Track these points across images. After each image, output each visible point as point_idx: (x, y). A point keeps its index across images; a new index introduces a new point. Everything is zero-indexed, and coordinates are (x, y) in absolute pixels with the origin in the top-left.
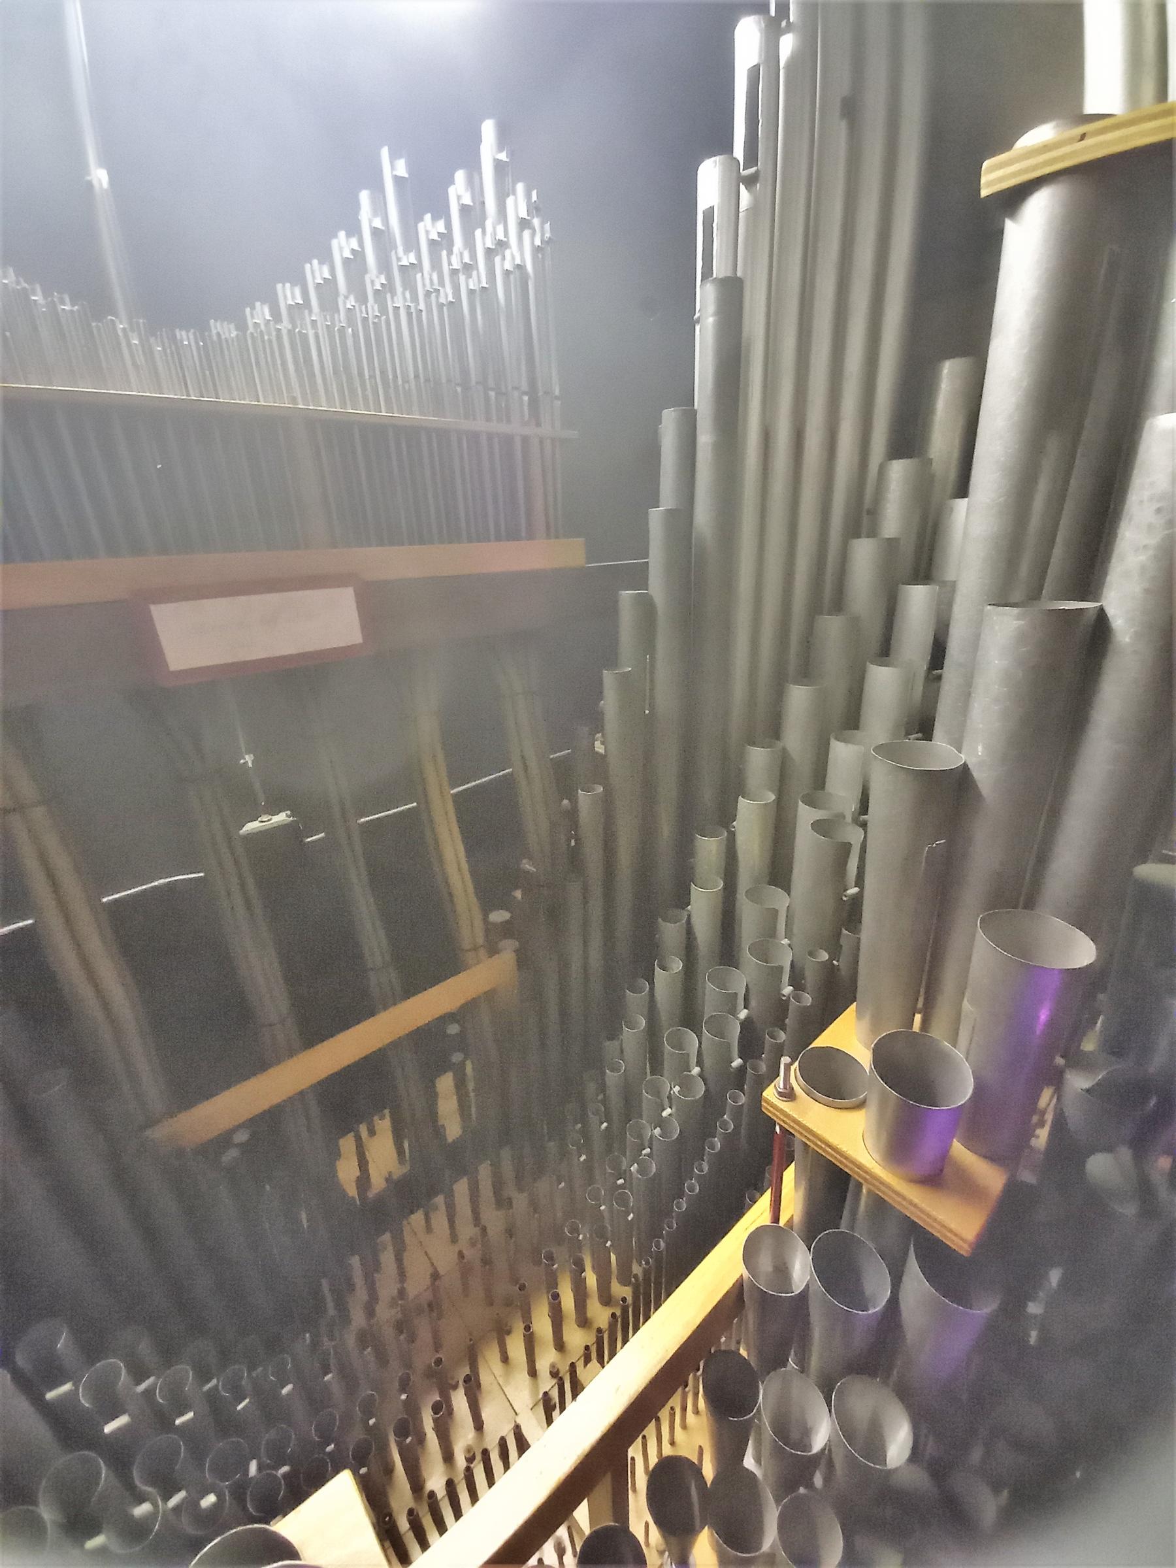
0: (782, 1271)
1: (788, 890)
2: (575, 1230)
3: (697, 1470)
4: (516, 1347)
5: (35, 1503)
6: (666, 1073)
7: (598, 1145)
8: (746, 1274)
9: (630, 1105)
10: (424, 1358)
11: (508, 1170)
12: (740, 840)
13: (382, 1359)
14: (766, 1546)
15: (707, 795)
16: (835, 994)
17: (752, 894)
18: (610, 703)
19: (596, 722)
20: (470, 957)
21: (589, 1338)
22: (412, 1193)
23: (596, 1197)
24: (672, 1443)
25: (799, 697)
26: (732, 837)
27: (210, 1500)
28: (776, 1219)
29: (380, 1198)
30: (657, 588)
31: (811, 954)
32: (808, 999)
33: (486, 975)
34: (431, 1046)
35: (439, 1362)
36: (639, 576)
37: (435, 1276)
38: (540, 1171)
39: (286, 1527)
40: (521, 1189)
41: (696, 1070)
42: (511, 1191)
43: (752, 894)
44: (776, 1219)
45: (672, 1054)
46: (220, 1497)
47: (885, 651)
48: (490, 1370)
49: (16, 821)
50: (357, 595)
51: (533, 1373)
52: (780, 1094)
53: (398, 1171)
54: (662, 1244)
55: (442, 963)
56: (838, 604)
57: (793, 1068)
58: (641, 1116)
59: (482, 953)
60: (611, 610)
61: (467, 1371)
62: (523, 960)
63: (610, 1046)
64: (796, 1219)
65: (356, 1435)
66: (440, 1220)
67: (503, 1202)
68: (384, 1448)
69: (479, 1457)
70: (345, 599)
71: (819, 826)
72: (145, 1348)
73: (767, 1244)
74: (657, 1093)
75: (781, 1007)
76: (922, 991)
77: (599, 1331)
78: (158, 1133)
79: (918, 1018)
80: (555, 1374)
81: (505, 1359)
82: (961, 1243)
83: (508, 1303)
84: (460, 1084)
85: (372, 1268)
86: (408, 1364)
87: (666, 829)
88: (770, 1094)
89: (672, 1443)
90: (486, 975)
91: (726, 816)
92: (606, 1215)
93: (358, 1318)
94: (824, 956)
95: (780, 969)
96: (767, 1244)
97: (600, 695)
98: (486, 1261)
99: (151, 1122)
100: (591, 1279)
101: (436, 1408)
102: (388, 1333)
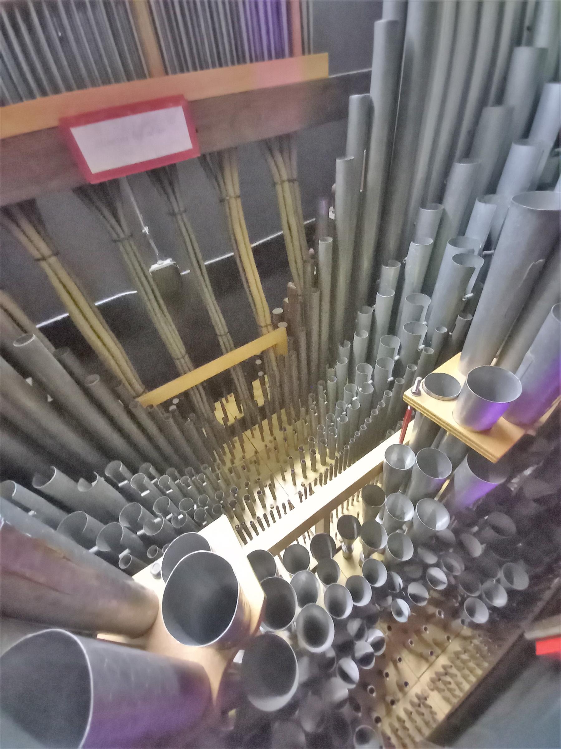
0: (401, 461)
1: (430, 295)
2: (312, 440)
3: (357, 520)
4: (288, 476)
5: (117, 520)
6: (356, 382)
7: (322, 410)
8: (385, 461)
9: (338, 397)
10: (254, 477)
11: (284, 417)
12: (408, 268)
13: (239, 477)
14: (382, 547)
15: (392, 243)
16: (448, 348)
17: (411, 298)
18: (339, 186)
19: (331, 198)
20: (264, 330)
21: (317, 475)
22: (245, 424)
23: (321, 428)
24: (348, 509)
25: (461, 171)
26: (403, 266)
27: (181, 516)
28: (402, 441)
29: (233, 425)
30: (377, 91)
31: (438, 329)
32: (432, 351)
33: (272, 339)
34: (251, 369)
35: (259, 479)
36: (362, 83)
37: (256, 452)
38: (298, 418)
39: (202, 533)
40: (290, 424)
41: (371, 382)
42: (285, 425)
43: (411, 298)
44: (402, 441)
45: (359, 374)
46: (185, 516)
47: (526, 134)
48: (278, 482)
49: (43, 264)
50: (183, 108)
51: (295, 484)
52: (413, 393)
53: (239, 416)
54: (349, 447)
55: (245, 331)
56: (500, 100)
57: (422, 381)
58: (343, 399)
59: (270, 328)
60: (342, 114)
61: (269, 482)
62: (290, 331)
63: (330, 371)
64: (411, 443)
65: (231, 499)
66: (257, 433)
67: (281, 428)
68: (241, 503)
69: (275, 508)
70: (177, 116)
71: (458, 258)
72: (152, 470)
73: (396, 450)
74: (351, 391)
75: (418, 354)
76: (502, 346)
77: (321, 474)
78: (140, 399)
79: (495, 360)
80: (303, 485)
81: (284, 479)
82: (493, 458)
83: (285, 462)
84: (263, 383)
85: (232, 449)
86: (248, 478)
87: (366, 264)
88: (408, 393)
89: (348, 509)
90: (272, 339)
91: (401, 253)
92: (326, 436)
93: (229, 464)
94: (445, 330)
95: (420, 337)
96: (396, 450)
97: (334, 181)
98: (275, 448)
99: (139, 395)
100: (318, 456)
101: (259, 493)
102: (240, 469)
